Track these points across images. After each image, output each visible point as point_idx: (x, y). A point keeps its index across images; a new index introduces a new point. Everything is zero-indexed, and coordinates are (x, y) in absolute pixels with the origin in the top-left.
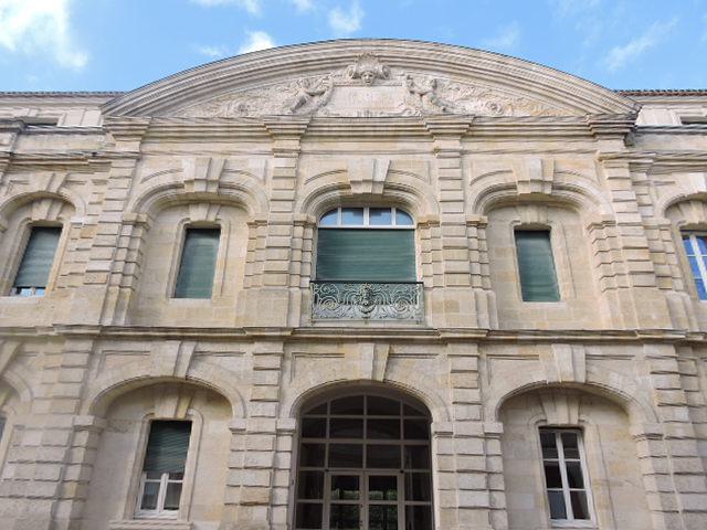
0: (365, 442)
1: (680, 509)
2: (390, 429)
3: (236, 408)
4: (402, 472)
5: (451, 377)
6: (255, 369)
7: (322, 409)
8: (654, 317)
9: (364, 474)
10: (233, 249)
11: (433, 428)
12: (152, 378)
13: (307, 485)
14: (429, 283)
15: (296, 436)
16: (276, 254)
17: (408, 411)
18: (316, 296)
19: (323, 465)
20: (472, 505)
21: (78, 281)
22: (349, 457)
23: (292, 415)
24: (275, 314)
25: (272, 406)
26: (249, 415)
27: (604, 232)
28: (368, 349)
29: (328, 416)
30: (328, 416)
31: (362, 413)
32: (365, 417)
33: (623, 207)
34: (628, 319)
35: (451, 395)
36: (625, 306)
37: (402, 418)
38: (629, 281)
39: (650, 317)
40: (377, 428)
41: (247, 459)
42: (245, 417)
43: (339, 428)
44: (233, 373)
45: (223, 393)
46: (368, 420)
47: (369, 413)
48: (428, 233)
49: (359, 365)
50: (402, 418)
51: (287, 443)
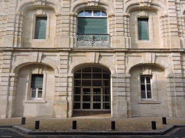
0: (92, 79)
1: (117, 86)
2: (99, 76)
3: (56, 71)
4: (102, 87)
5: (117, 62)
6: (61, 60)
7: (80, 71)
8: (176, 45)
9: (92, 88)
10: (52, 24)
12: (30, 63)
13: (76, 91)
14: (111, 34)
15: (73, 78)
16: (65, 25)
17: (104, 71)
18: (78, 38)
19: (80, 86)
21: (5, 34)
22: (88, 83)
23: (72, 72)
24: (65, 44)
25: (66, 70)
26: (60, 72)
27: (165, 19)
28: (93, 54)
30: (82, 73)
32: (92, 73)
33: (171, 11)
34: (168, 45)
36: (168, 41)
37: (92, 73)
38: (170, 34)
39: (175, 45)
40: (95, 76)
42: (58, 73)
43: (85, 76)
44: (54, 61)
45: (52, 66)
47: (93, 72)
48: (112, 19)
49: (90, 58)
50: (102, 73)
51: (71, 80)
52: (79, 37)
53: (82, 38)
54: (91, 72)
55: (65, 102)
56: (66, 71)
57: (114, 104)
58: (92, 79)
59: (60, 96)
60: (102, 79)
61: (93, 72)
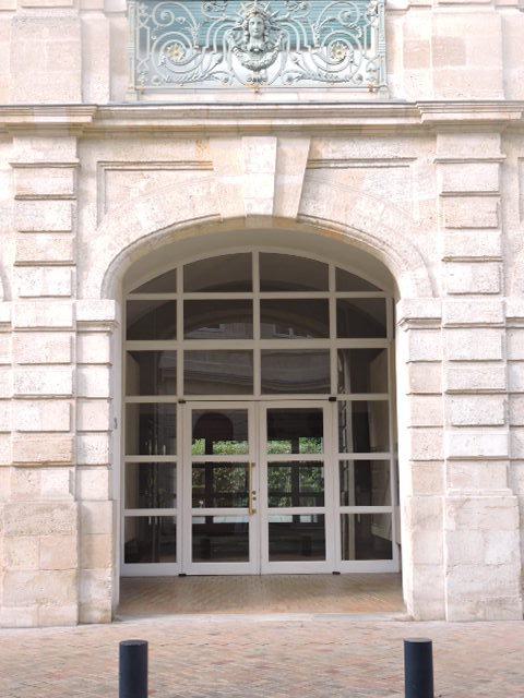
0: (257, 344)
2: (309, 318)
4: (332, 400)
5: (439, 206)
6: (19, 198)
7: (165, 282)
9: (257, 407)
11: (401, 313)
13: (145, 429)
15: (119, 333)
17: (346, 280)
18: (143, 31)
19: (174, 393)
20: (476, 454)
23: (106, 293)
28: (265, 148)
29: (180, 297)
30: (180, 297)
31: (249, 288)
32: (256, 296)
35: (439, 243)
37: (256, 296)
40: (281, 318)
41: (20, 381)
43: (202, 317)
46: (263, 302)
47: (263, 288)
49: (245, 185)
50: (332, 295)
52: (150, 24)
53: (177, 26)
54: (249, 288)
55: (64, 507)
56: (59, 279)
57: (420, 522)
58: (257, 344)
59: (21, 466)
60: (334, 343)
61: (263, 288)
